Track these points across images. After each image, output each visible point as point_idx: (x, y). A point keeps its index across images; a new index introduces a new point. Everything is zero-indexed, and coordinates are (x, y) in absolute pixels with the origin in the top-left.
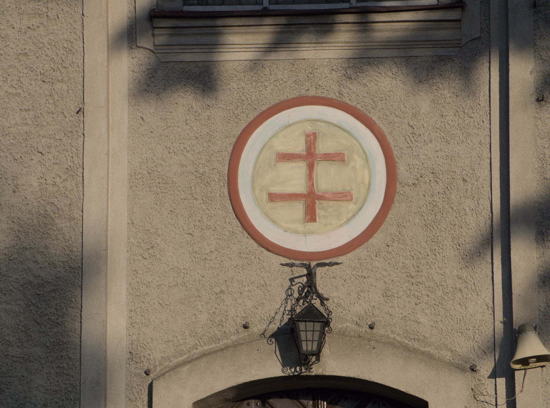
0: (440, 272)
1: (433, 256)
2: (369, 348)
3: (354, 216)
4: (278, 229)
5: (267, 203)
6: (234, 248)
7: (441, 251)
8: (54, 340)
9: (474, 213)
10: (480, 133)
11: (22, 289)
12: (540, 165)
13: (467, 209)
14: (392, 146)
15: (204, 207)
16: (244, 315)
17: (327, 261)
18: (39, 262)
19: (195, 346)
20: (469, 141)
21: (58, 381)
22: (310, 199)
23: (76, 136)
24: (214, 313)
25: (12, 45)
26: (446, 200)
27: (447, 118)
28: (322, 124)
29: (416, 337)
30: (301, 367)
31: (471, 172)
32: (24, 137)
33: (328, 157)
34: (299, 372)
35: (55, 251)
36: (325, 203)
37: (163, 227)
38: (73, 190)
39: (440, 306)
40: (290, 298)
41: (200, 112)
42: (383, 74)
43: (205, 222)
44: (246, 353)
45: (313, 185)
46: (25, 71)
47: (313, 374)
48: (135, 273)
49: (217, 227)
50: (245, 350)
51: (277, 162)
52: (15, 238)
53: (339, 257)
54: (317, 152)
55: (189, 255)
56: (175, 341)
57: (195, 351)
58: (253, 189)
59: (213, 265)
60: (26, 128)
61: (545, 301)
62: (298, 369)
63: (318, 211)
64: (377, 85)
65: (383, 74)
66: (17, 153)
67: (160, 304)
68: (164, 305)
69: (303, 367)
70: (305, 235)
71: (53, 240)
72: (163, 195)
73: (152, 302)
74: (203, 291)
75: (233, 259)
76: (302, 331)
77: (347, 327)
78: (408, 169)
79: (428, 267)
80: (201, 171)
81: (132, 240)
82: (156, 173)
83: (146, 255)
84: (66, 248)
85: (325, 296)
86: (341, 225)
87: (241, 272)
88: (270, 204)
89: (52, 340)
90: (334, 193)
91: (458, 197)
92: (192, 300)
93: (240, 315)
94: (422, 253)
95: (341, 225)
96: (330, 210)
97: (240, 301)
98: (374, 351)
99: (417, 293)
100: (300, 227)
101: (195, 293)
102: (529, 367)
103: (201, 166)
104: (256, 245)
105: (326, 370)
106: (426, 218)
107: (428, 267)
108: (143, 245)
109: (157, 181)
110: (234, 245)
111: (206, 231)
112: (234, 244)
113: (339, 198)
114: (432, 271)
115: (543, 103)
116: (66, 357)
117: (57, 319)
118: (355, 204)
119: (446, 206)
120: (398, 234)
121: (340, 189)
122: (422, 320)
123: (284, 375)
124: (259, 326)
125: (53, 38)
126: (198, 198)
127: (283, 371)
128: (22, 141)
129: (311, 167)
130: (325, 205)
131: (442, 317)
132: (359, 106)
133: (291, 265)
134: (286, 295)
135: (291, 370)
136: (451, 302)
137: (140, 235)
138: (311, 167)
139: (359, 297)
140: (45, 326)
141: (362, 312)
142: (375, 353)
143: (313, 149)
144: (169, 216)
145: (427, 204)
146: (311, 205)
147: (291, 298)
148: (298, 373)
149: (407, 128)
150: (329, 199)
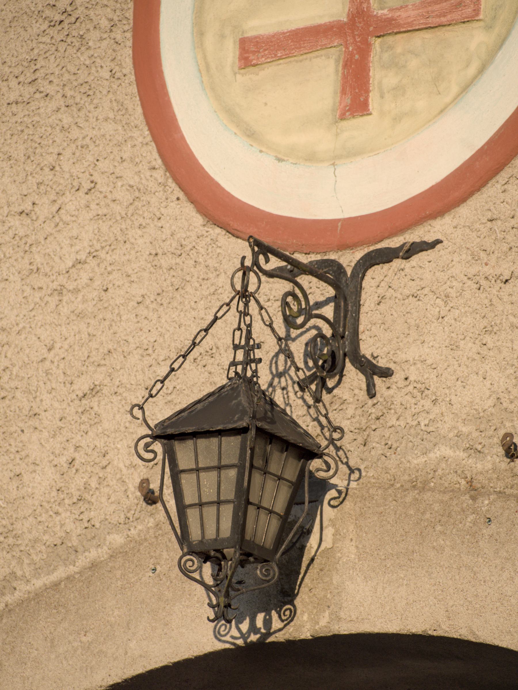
2: (475, 523)
4: (260, 155)
5: (235, 74)
6: (140, 241)
15: (67, 120)
17: (394, 243)
22: (354, 37)
30: (268, 613)
34: (263, 631)
40: (280, 382)
44: (119, 583)
47: (306, 634)
49: (99, 181)
50: (119, 573)
53: (434, 223)
59: (80, 306)
62: (260, 618)
69: (274, 613)
70: (333, 164)
74: (45, 396)
75: (134, 278)
77: (444, 458)
85: (382, 363)
88: (243, 75)
92: (13, 429)
95: (442, 111)
96: (413, 63)
104: (198, 220)
105: (342, 615)
110: (140, 232)
112: (140, 226)
113: (439, 16)
118: (489, 28)
123: (219, 646)
126: (52, 93)
127: (217, 635)
130: (399, 50)
134: (272, 373)
135: (241, 626)
142: (491, 536)
146: (357, 57)
147: (283, 384)
148: (258, 636)
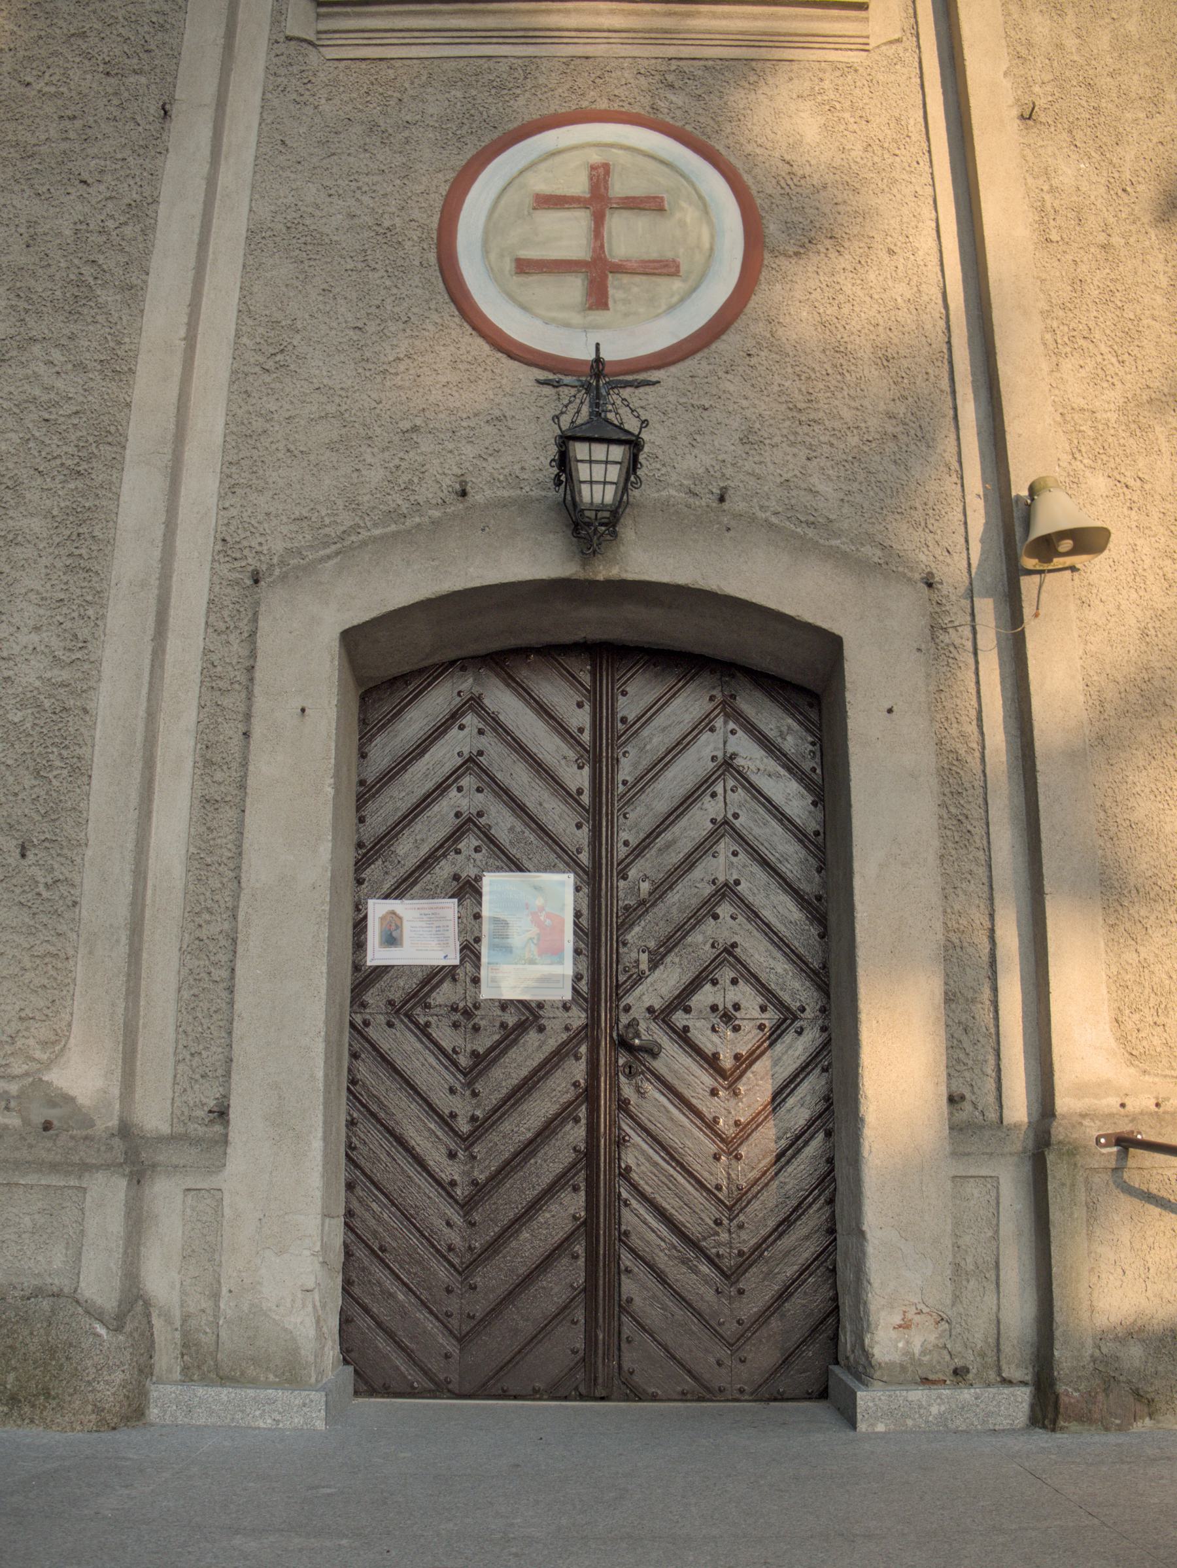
0: (853, 404)
1: (839, 377)
2: (719, 529)
3: (682, 300)
7: (853, 368)
8: (68, 503)
9: (912, 307)
10: (913, 180)
11: (18, 411)
12: (1037, 218)
13: (899, 300)
14: (754, 192)
15: (388, 283)
16: (459, 472)
17: (630, 378)
18: (56, 362)
19: (355, 529)
20: (895, 191)
21: (66, 583)
23: (153, 153)
24: (397, 467)
25: (61, 23)
26: (859, 282)
27: (853, 153)
28: (621, 152)
29: (812, 519)
31: (903, 239)
32: (60, 159)
33: (633, 204)
35: (88, 343)
36: (626, 279)
37: (307, 316)
38: (135, 239)
39: (856, 464)
41: (390, 131)
42: (732, 84)
43: (389, 308)
45: (602, 247)
46: (78, 59)
48: (245, 396)
51: (534, 209)
52: (18, 324)
54: (611, 194)
55: (353, 366)
56: (313, 519)
57: (353, 538)
58: (486, 251)
60: (65, 146)
61: (1068, 448)
63: (611, 291)
64: (721, 98)
65: (732, 84)
66: (43, 185)
67: (288, 450)
68: (296, 452)
71: (88, 324)
72: (312, 263)
73: (274, 447)
74: (376, 428)
76: (582, 461)
77: (670, 496)
78: (784, 228)
79: (829, 394)
80: (387, 224)
81: (245, 340)
82: (301, 228)
83: (270, 364)
84: (109, 337)
86: (658, 316)
87: (456, 394)
89: (63, 505)
90: (643, 261)
91: (881, 278)
93: (449, 472)
94: (817, 369)
97: (450, 446)
98: (728, 535)
99: (808, 439)
100: (576, 318)
101: (361, 431)
102: (1050, 568)
103: (386, 216)
104: (486, 347)
106: (821, 311)
107: (829, 394)
108: (264, 347)
109: (303, 240)
111: (390, 323)
114: (836, 402)
115: (1031, 122)
116: (87, 536)
117: (78, 464)
118: (684, 281)
119: (860, 293)
120: (769, 335)
121: (654, 255)
122: (821, 487)
124: (488, 493)
125: (134, 10)
128: (54, 166)
129: (599, 220)
131: (861, 483)
132: (689, 128)
133: (556, 385)
136: (877, 458)
137: (261, 330)
138: (599, 220)
139: (694, 443)
140: (53, 478)
141: (701, 471)
143: (602, 190)
144: (321, 298)
145: (824, 286)
149: (780, 164)
150: (633, 273)
